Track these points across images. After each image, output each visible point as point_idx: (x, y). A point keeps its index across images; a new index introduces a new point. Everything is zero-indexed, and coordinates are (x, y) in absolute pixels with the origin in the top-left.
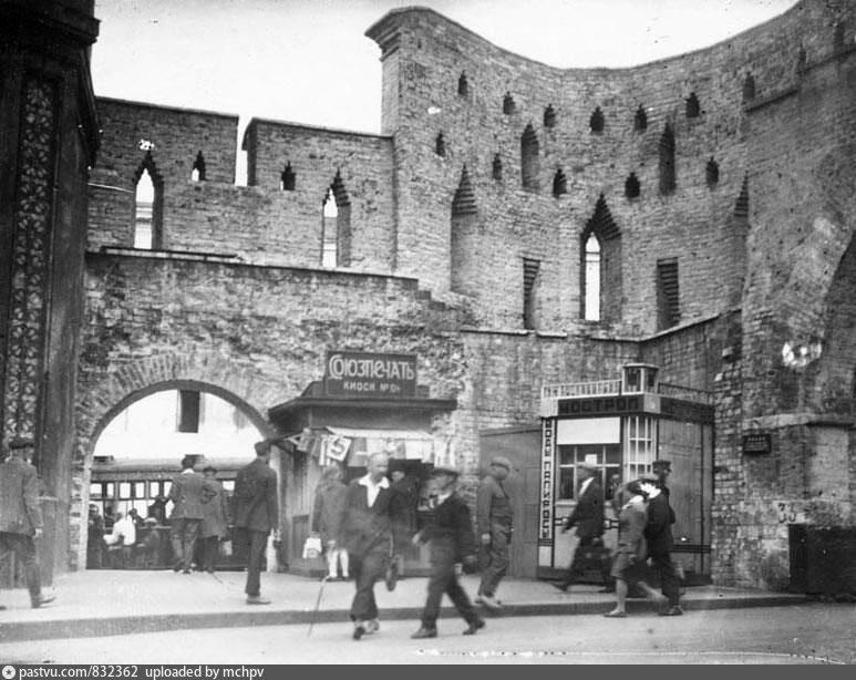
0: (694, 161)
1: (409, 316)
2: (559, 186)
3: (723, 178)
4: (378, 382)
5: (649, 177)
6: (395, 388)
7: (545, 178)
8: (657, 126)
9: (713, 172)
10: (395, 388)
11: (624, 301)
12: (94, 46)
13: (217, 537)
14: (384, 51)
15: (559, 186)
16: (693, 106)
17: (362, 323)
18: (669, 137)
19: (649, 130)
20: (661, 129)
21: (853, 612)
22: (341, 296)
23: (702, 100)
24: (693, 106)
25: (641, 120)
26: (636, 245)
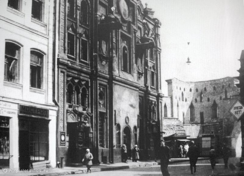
0: (205, 97)
1: (178, 123)
2: (186, 101)
3: (210, 101)
4: (181, 134)
5: (198, 99)
6: (183, 134)
7: (185, 100)
8: (200, 91)
9: (209, 100)
10: (183, 134)
11: (195, 118)
12: (239, 67)
13: (69, 124)
14: (131, 74)
15: (186, 101)
16: (205, 89)
17: (172, 125)
18: (201, 93)
19: (198, 92)
20: (200, 92)
21: (203, 147)
22: (170, 121)
23: (207, 88)
24: (205, 89)
25: (197, 90)
26: (197, 109)
